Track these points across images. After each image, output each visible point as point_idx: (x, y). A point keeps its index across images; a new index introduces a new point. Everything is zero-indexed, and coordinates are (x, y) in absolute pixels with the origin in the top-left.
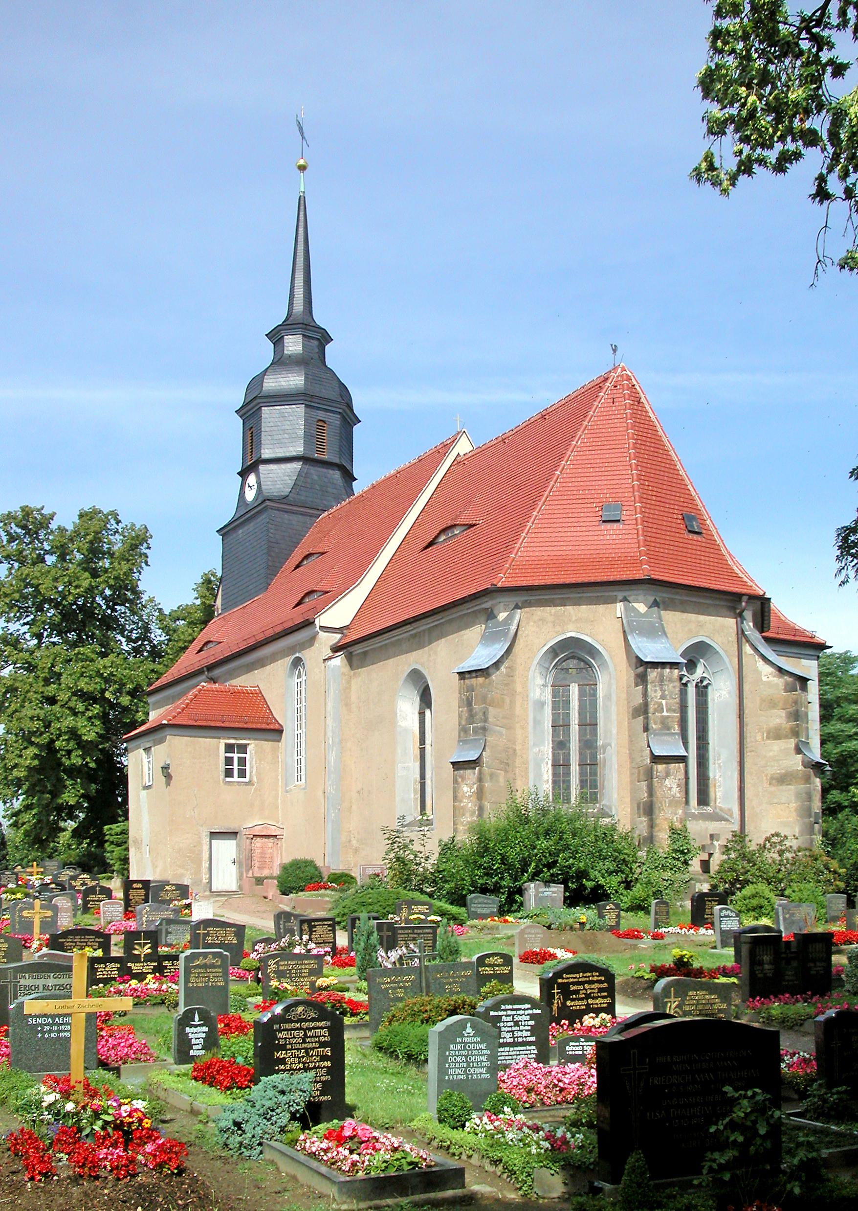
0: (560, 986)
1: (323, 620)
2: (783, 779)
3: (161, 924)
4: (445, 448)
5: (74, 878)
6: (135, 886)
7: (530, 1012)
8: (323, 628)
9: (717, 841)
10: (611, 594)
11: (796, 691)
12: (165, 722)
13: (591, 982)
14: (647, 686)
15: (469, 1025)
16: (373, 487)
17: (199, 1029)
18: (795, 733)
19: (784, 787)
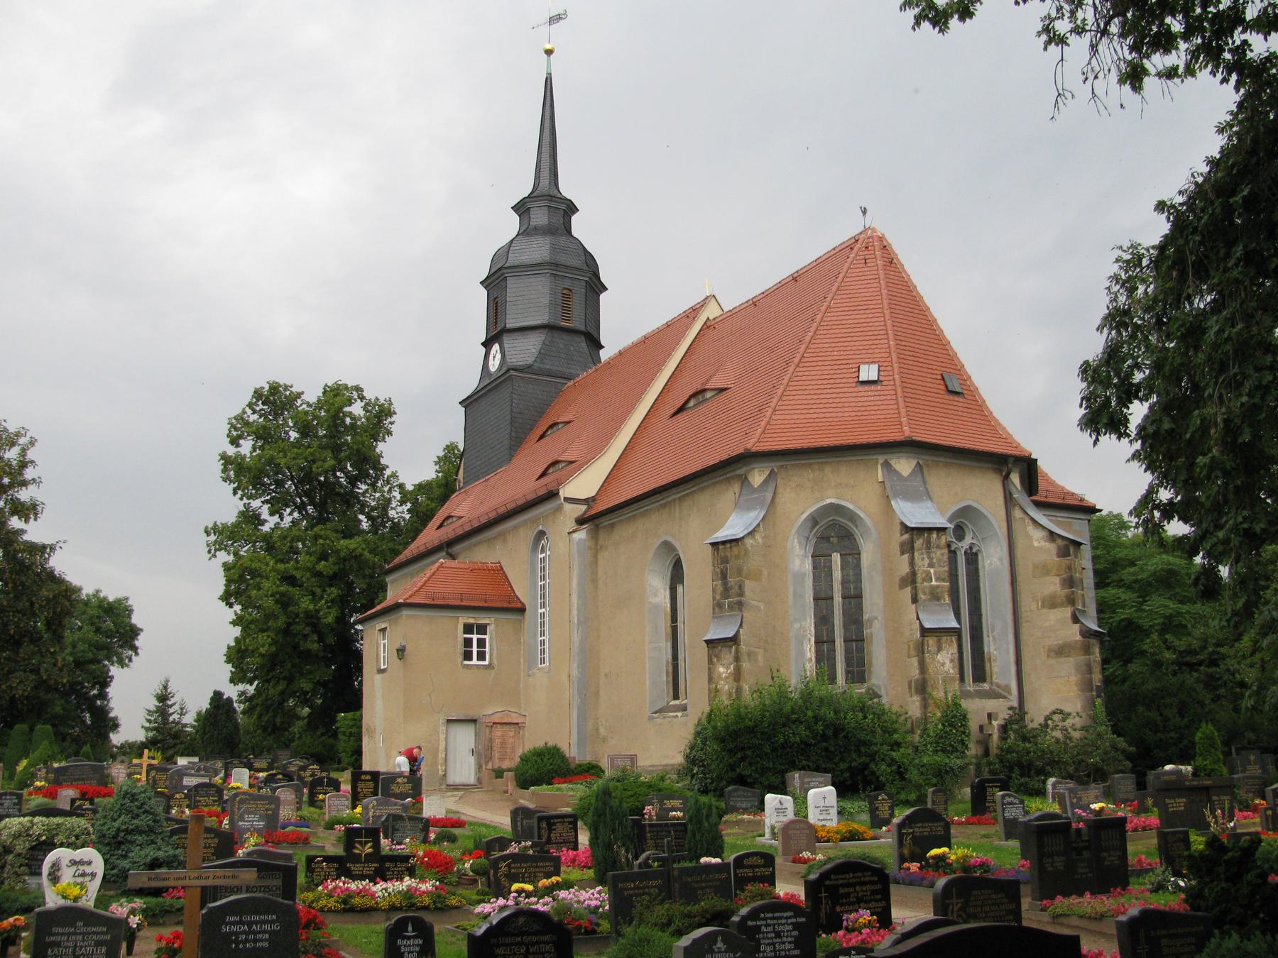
0: (828, 889)
1: (568, 491)
2: (1061, 651)
3: (387, 819)
4: (694, 311)
5: (303, 768)
6: (363, 777)
7: (793, 920)
8: (566, 499)
9: (996, 720)
10: (871, 457)
11: (1069, 555)
12: (401, 601)
13: (862, 884)
14: (913, 553)
15: (719, 938)
16: (620, 353)
17: (412, 941)
18: (1071, 601)
19: (1062, 660)
